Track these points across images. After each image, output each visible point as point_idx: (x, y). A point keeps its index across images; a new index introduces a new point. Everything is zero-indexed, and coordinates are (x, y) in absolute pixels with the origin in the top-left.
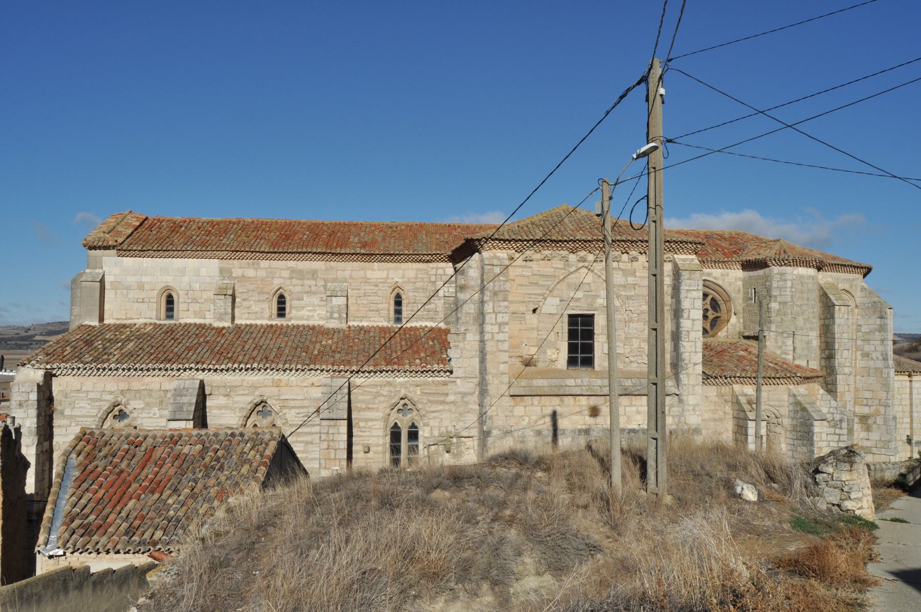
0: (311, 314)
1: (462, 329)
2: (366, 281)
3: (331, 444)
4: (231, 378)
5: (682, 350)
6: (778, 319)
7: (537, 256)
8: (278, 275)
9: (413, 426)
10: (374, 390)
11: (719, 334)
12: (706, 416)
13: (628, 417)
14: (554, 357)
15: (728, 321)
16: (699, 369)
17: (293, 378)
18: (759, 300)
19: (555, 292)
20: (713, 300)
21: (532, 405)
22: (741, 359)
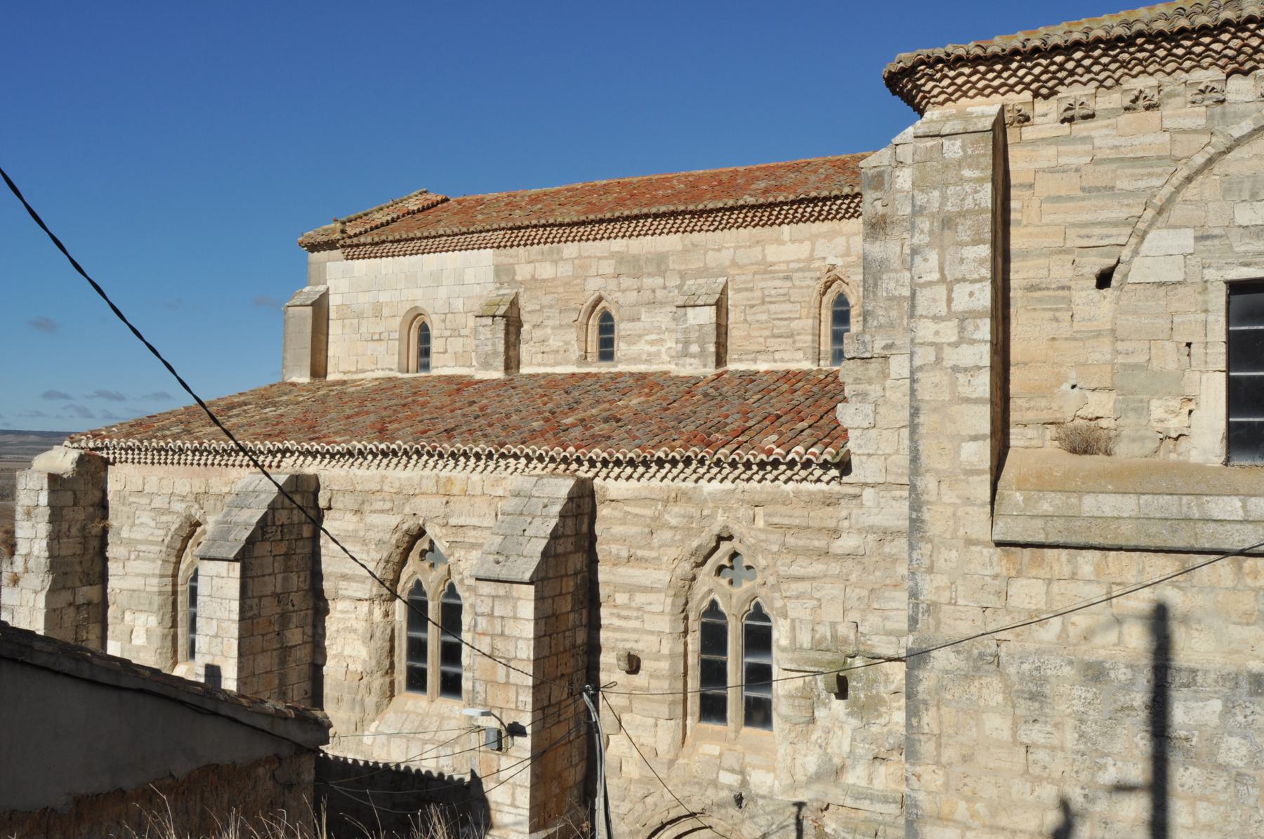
0: (653, 349)
1: (878, 346)
2: (766, 269)
3: (499, 644)
4: (362, 472)
7: (1115, 99)
8: (593, 271)
9: (758, 613)
10: (649, 512)
14: (1174, 425)
17: (476, 477)
19: (1178, 212)
21: (1073, 577)
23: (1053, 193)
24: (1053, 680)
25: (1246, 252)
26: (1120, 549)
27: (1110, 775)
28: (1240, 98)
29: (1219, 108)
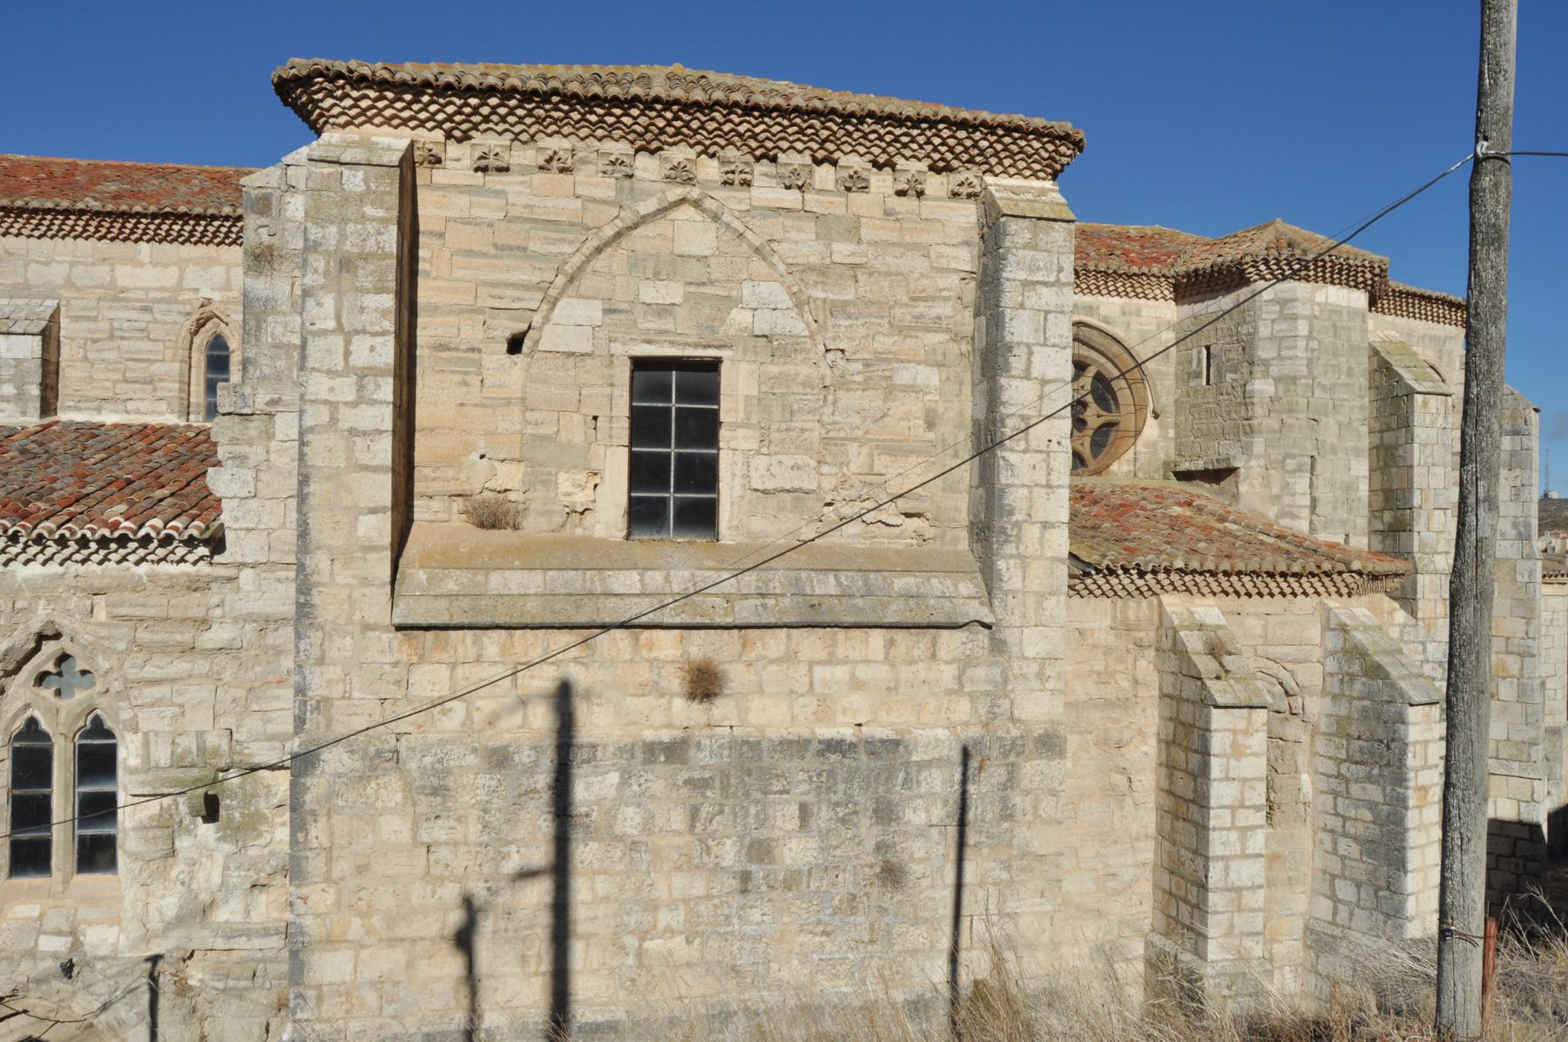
1: (261, 401)
2: (117, 295)
5: (1004, 478)
6: (1274, 423)
7: (524, 156)
9: (98, 728)
11: (1115, 467)
12: (1082, 690)
13: (823, 700)
14: (580, 499)
15: (1138, 433)
16: (1060, 543)
18: (1221, 369)
19: (587, 282)
21: (479, 659)
22: (1175, 524)
23: (465, 246)
25: (648, 330)
27: (512, 865)
28: (646, 175)
29: (627, 183)
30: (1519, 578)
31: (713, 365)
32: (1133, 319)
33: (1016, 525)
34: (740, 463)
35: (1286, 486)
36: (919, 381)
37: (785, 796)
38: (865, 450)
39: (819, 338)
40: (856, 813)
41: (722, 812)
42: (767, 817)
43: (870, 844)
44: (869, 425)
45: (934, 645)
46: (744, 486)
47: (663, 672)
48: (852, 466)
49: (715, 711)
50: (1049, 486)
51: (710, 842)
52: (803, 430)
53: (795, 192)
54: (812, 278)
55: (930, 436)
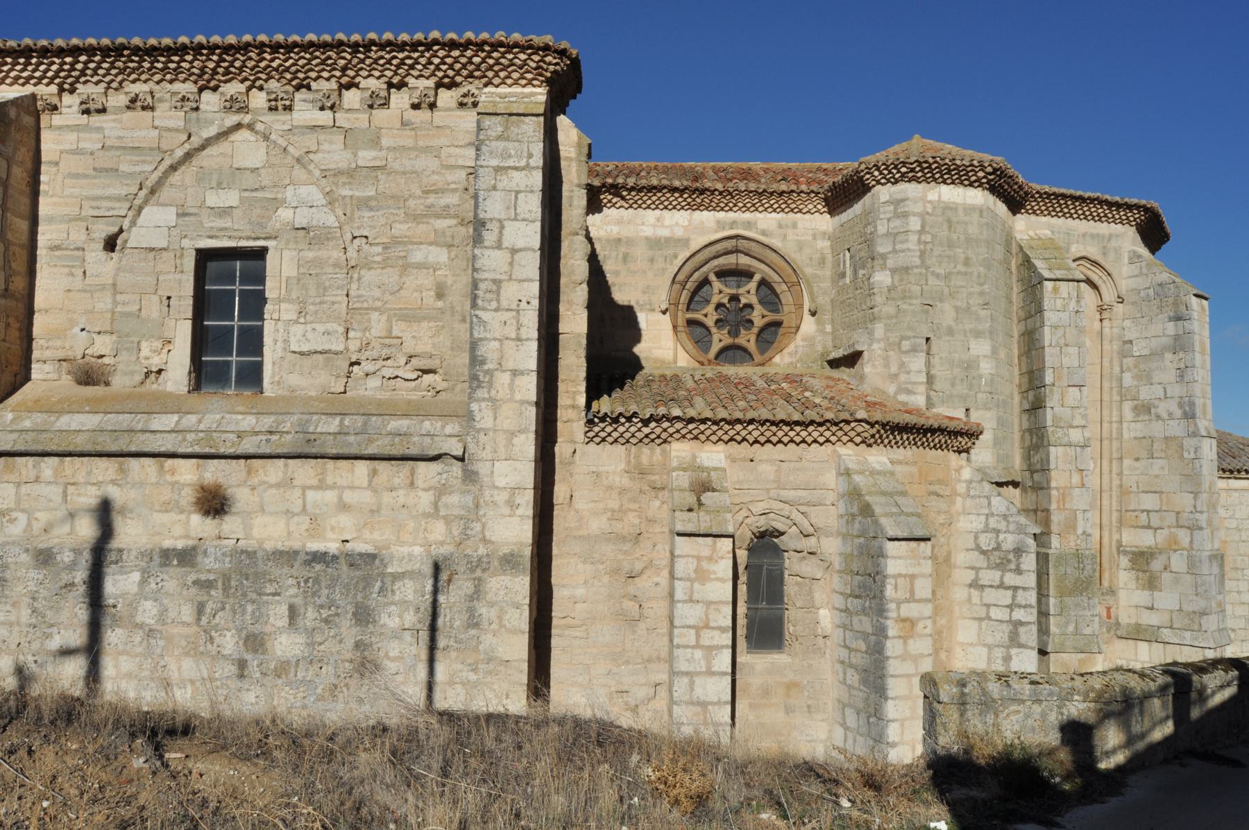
6: (890, 309)
7: (117, 100)
11: (777, 359)
14: (155, 363)
19: (165, 193)
20: (763, 283)
23: (73, 171)
24: (12, 566)
25: (212, 228)
26: (70, 455)
27: (56, 643)
28: (209, 108)
29: (194, 115)
30: (1186, 455)
31: (260, 254)
32: (790, 232)
33: (487, 372)
34: (284, 333)
35: (902, 365)
36: (431, 259)
37: (277, 598)
38: (384, 318)
39: (346, 228)
40: (337, 615)
41: (223, 609)
42: (261, 615)
43: (350, 643)
44: (387, 297)
45: (412, 475)
46: (285, 349)
47: (183, 493)
48: (373, 331)
49: (225, 526)
50: (519, 339)
51: (213, 633)
52: (333, 303)
53: (329, 113)
54: (343, 179)
55: (440, 304)
